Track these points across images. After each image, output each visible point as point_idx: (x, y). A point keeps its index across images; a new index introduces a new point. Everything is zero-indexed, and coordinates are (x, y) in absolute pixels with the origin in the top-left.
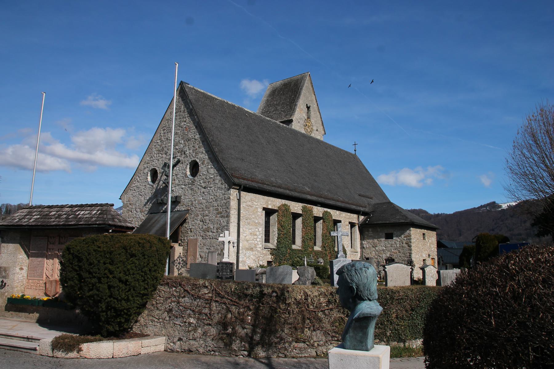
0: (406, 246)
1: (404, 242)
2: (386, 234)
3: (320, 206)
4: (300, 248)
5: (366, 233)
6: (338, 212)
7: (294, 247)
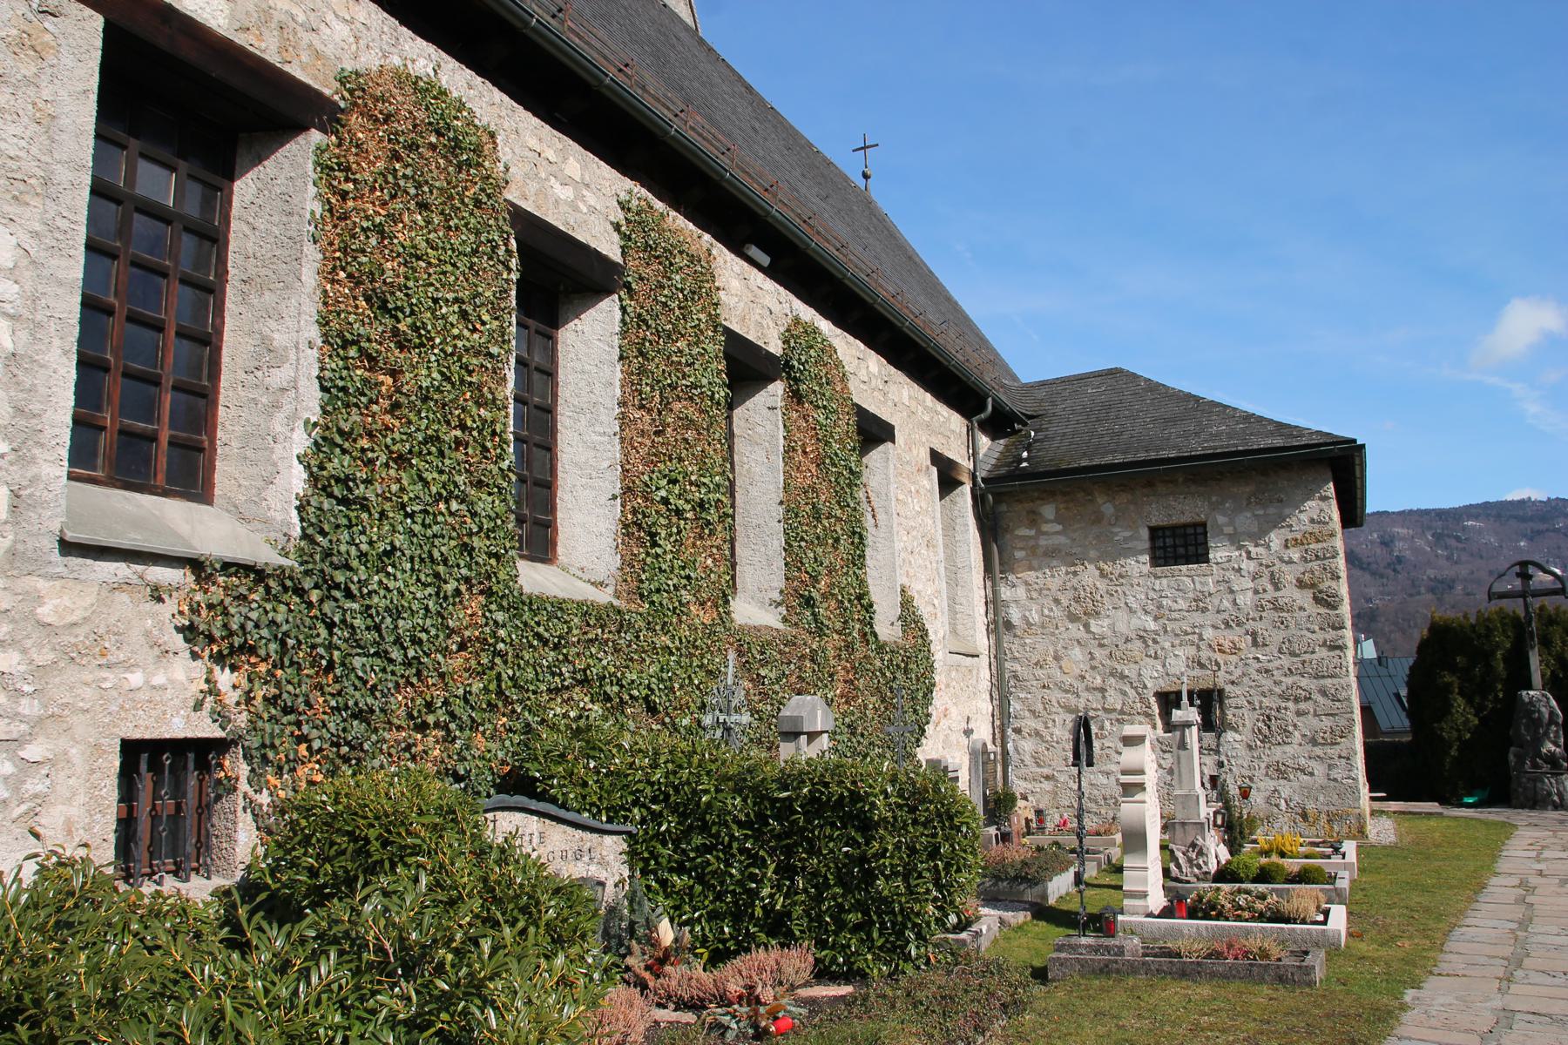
0: (1304, 598)
1: (1289, 575)
2: (1155, 532)
3: (765, 260)
4: (604, 597)
5: (1023, 532)
6: (874, 363)
7: (533, 578)
